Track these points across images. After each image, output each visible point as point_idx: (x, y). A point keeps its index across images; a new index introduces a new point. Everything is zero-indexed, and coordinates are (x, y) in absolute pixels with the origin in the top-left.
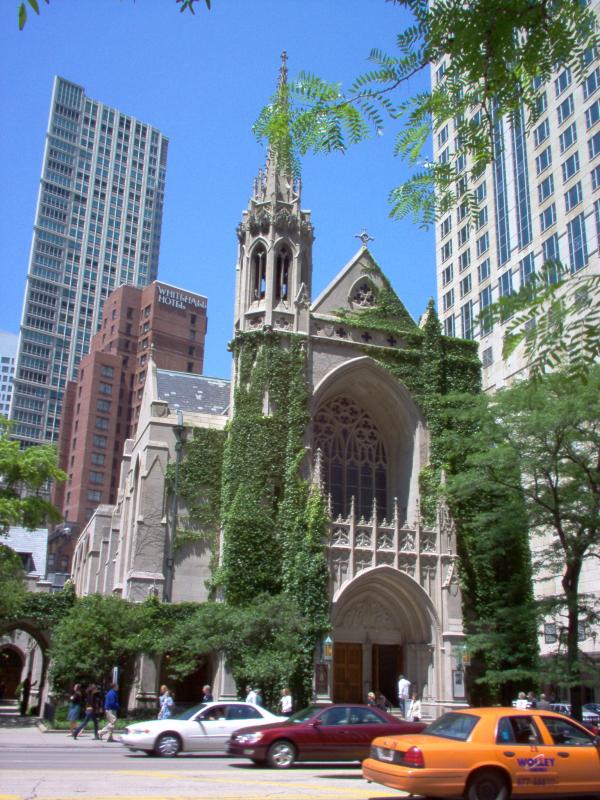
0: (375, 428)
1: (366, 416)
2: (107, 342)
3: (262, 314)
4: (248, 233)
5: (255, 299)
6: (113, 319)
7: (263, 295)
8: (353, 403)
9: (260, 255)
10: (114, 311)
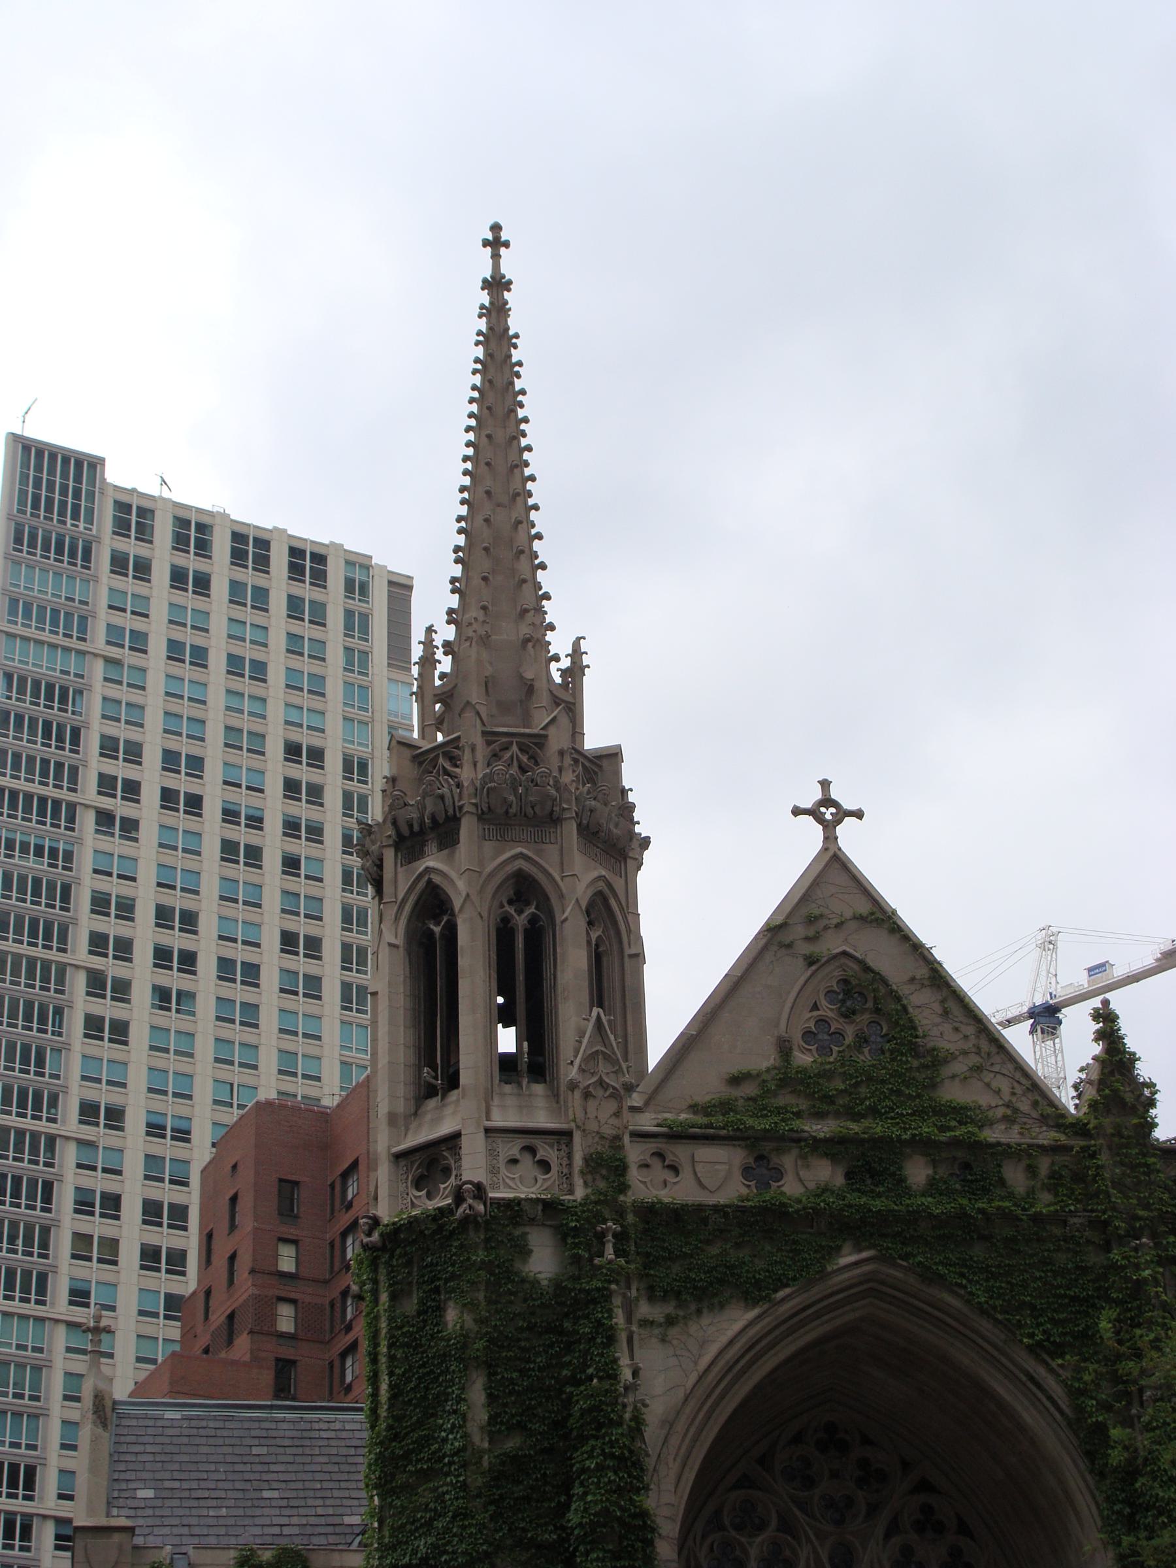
0: (963, 1529)
1: (923, 1486)
2: (218, 1317)
3: (453, 1140)
4: (389, 856)
5: (430, 1092)
6: (233, 1226)
7: (453, 1082)
9: (437, 930)
10: (234, 1200)
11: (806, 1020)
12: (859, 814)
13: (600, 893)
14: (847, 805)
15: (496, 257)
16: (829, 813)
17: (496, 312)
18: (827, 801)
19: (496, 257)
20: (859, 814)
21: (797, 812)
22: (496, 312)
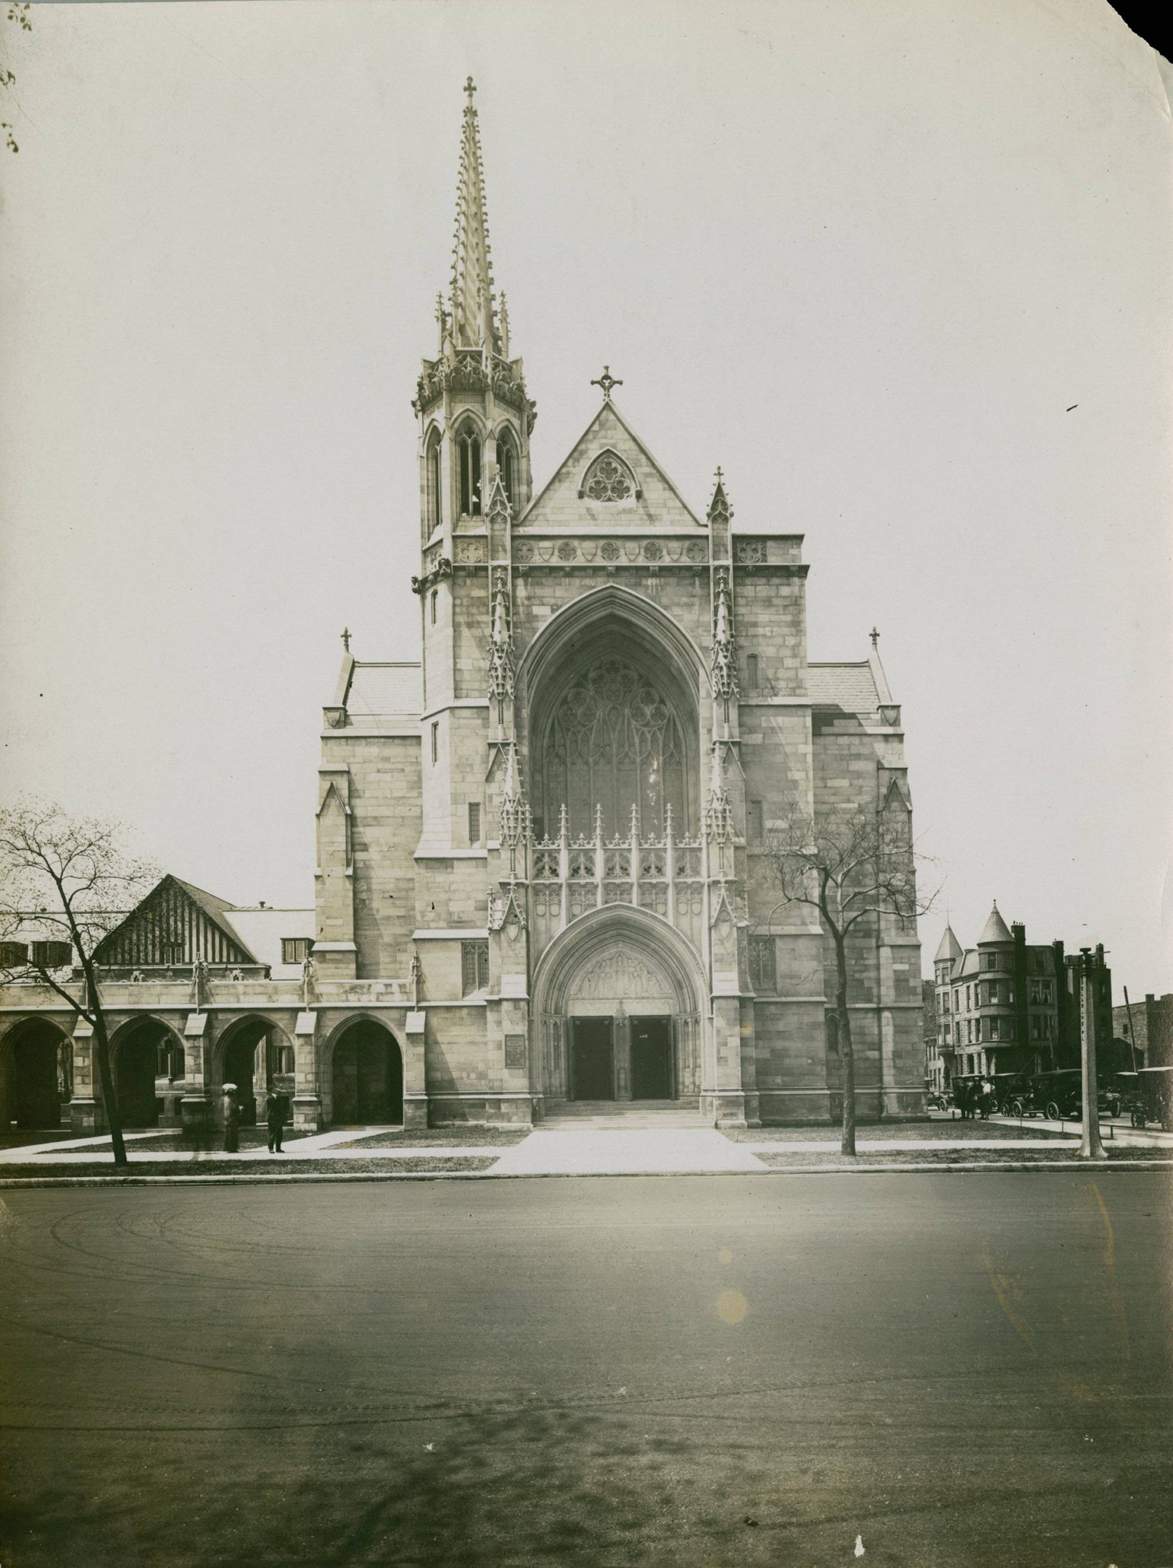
8: (626, 667)
11: (591, 482)
12: (621, 383)
13: (507, 427)
14: (615, 378)
15: (471, 96)
16: (607, 382)
17: (471, 130)
18: (606, 377)
19: (471, 96)
20: (621, 383)
21: (593, 383)
22: (471, 130)
